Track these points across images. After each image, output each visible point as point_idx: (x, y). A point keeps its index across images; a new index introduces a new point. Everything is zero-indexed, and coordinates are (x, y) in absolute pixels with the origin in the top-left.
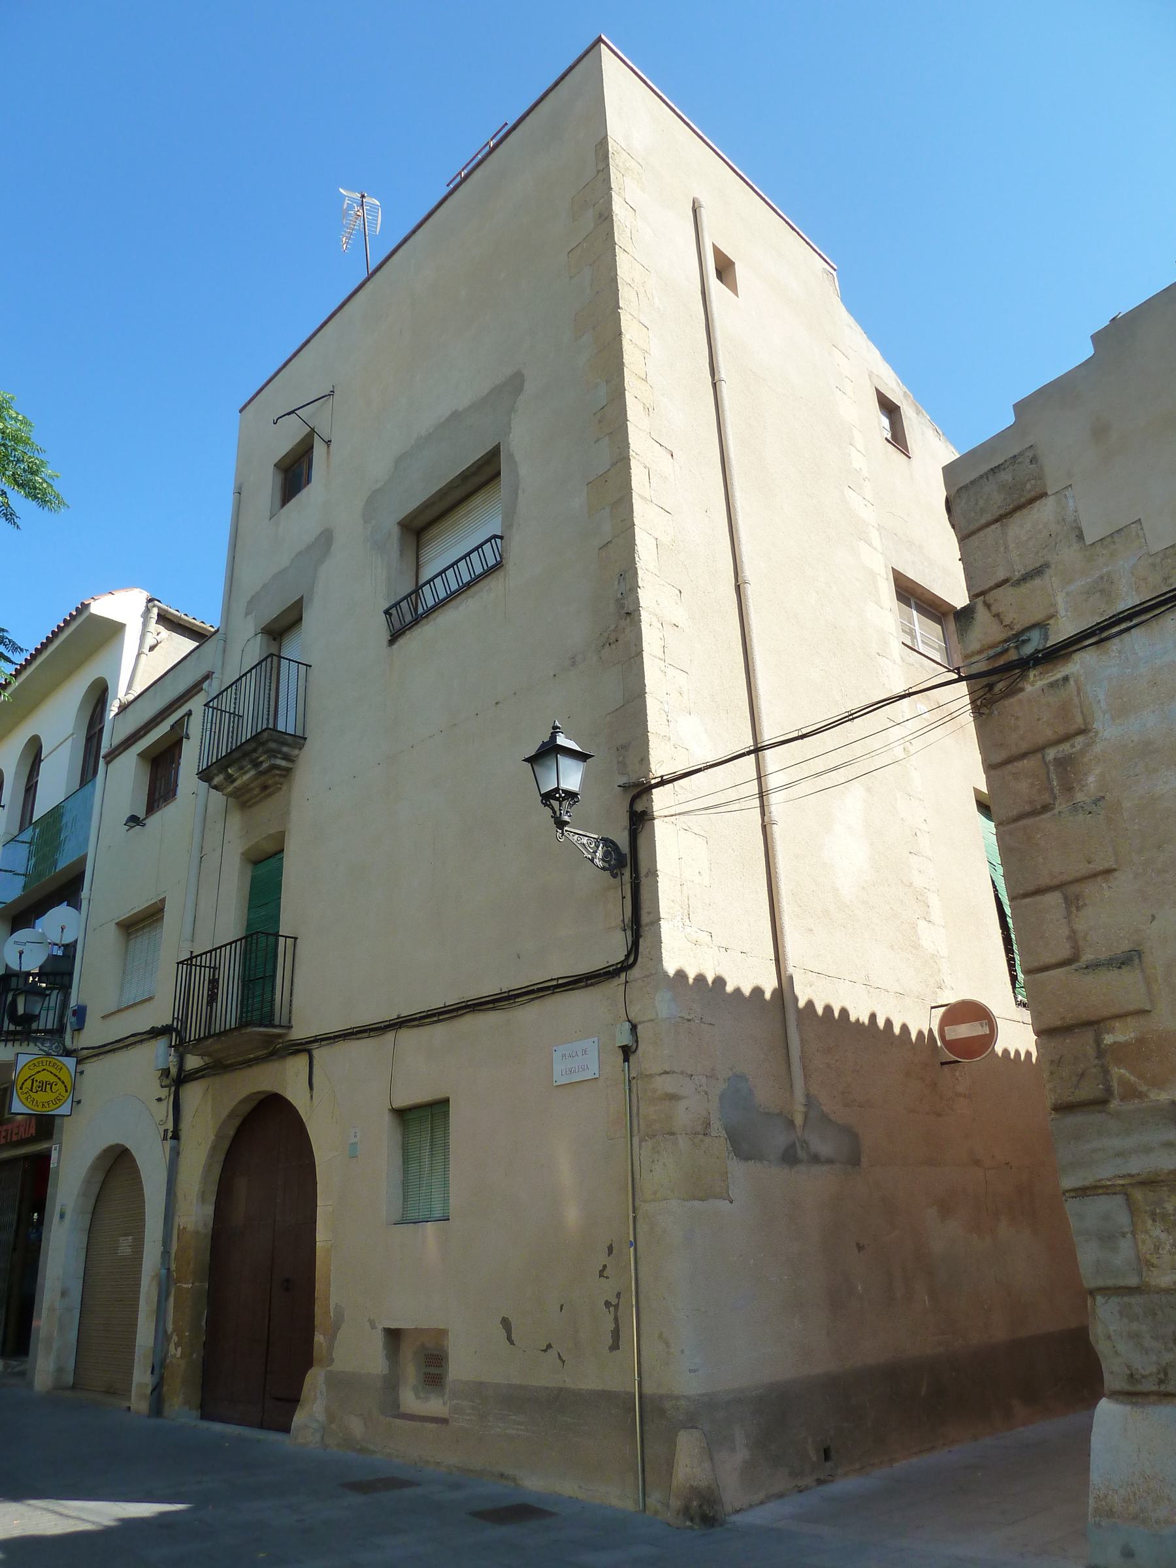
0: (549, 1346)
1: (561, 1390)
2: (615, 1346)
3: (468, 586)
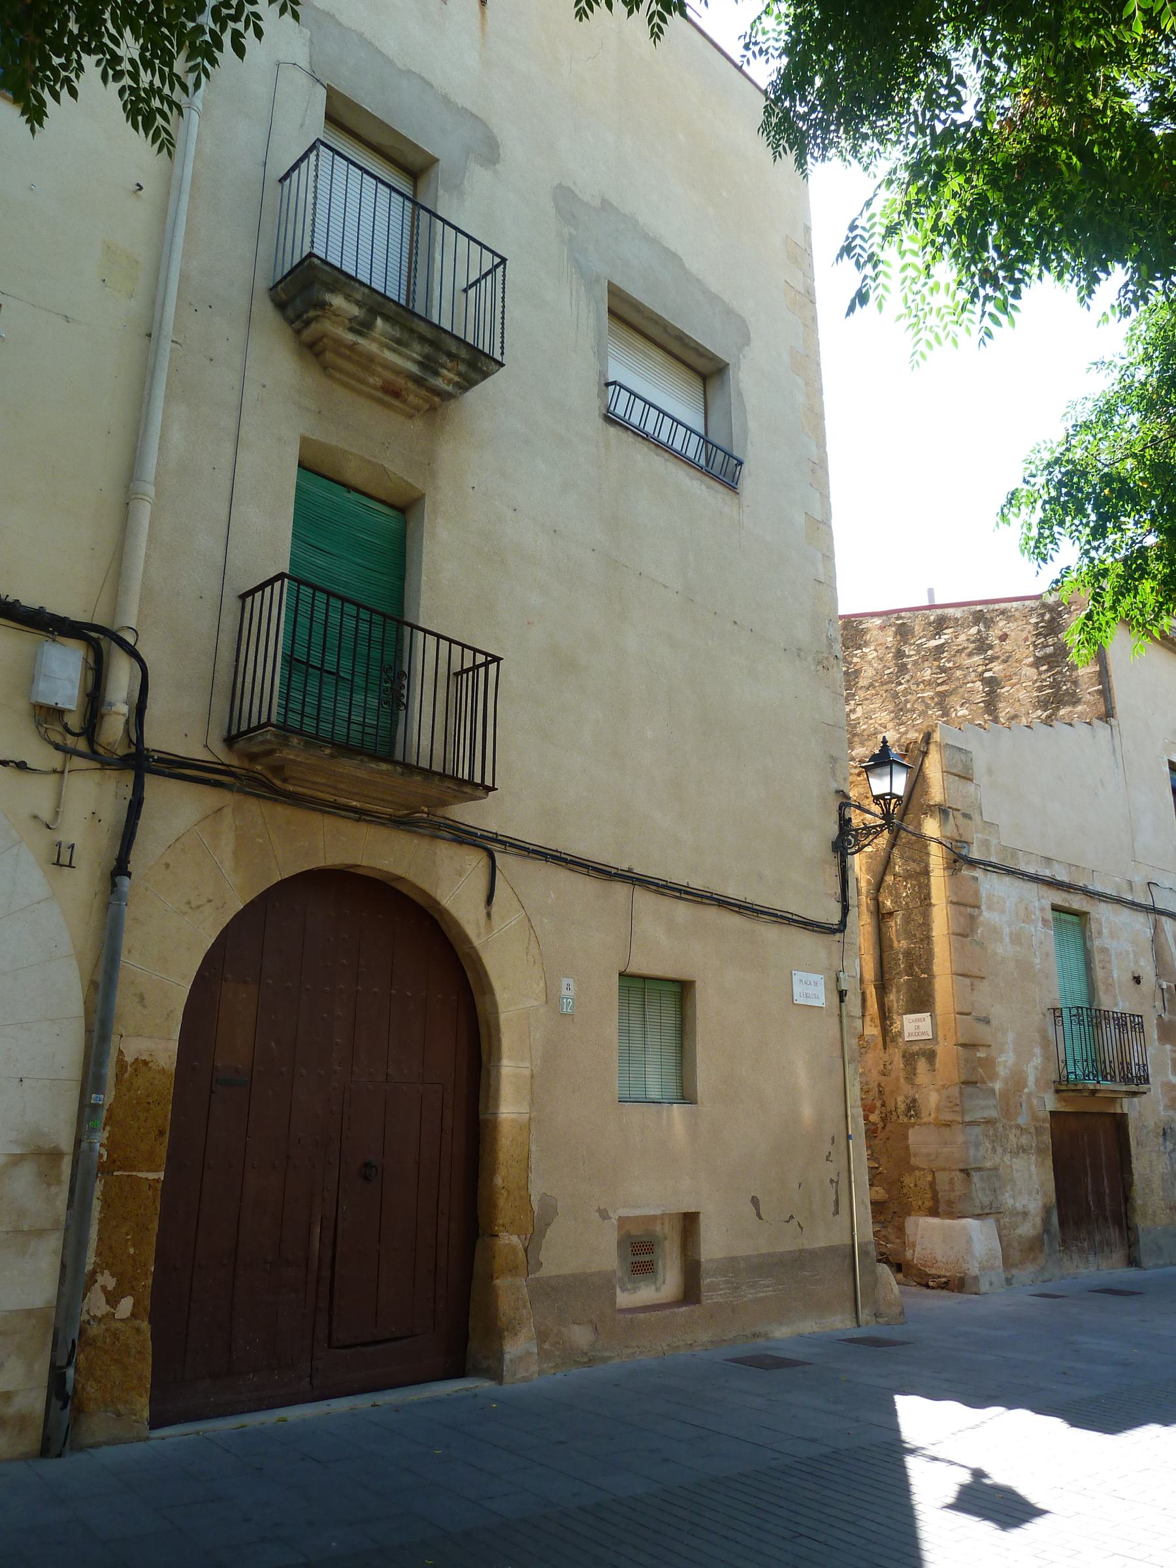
0: (792, 1217)
1: (801, 1251)
2: (837, 1212)
3: (646, 437)
